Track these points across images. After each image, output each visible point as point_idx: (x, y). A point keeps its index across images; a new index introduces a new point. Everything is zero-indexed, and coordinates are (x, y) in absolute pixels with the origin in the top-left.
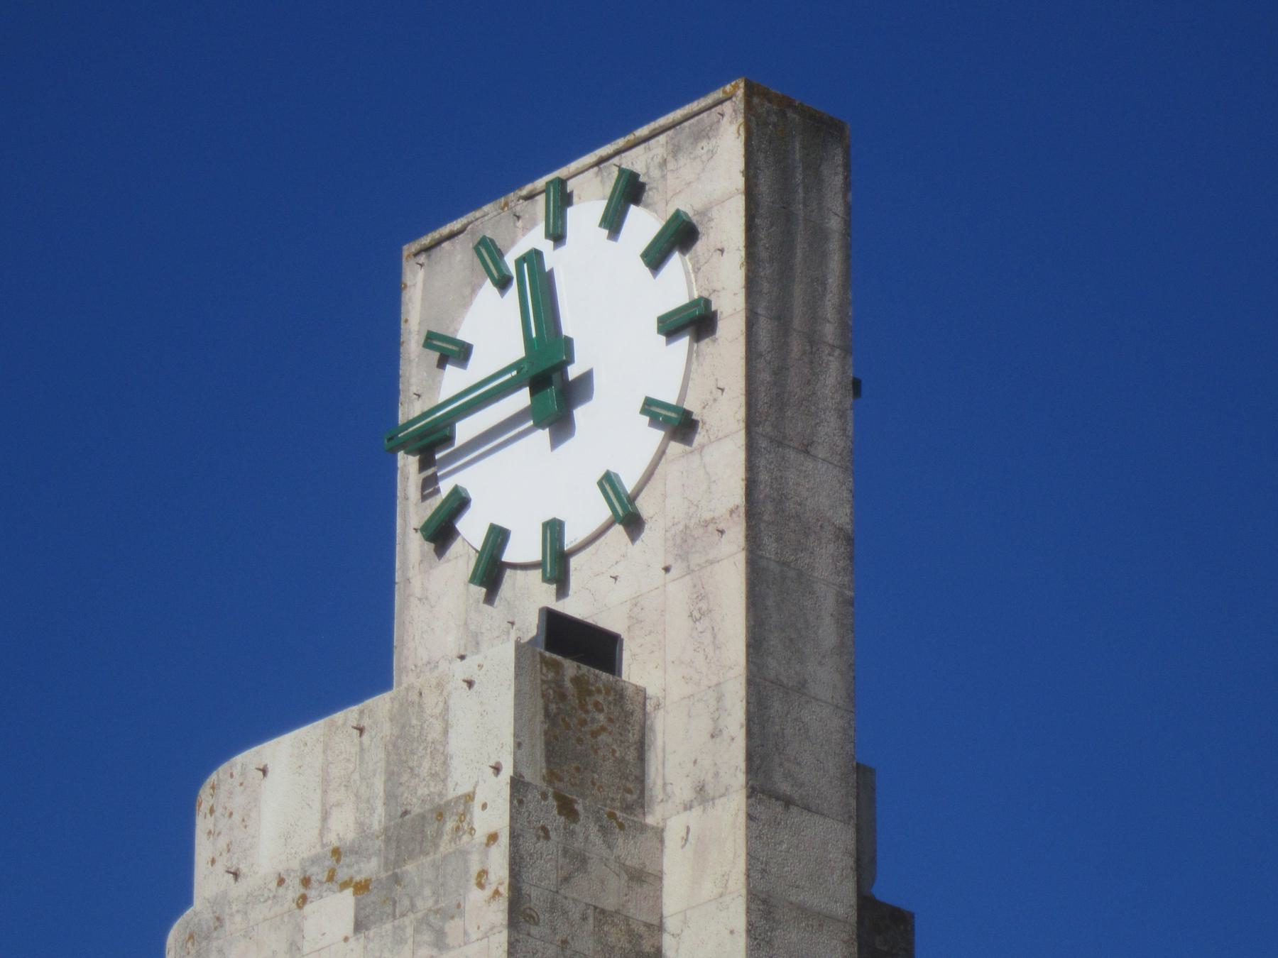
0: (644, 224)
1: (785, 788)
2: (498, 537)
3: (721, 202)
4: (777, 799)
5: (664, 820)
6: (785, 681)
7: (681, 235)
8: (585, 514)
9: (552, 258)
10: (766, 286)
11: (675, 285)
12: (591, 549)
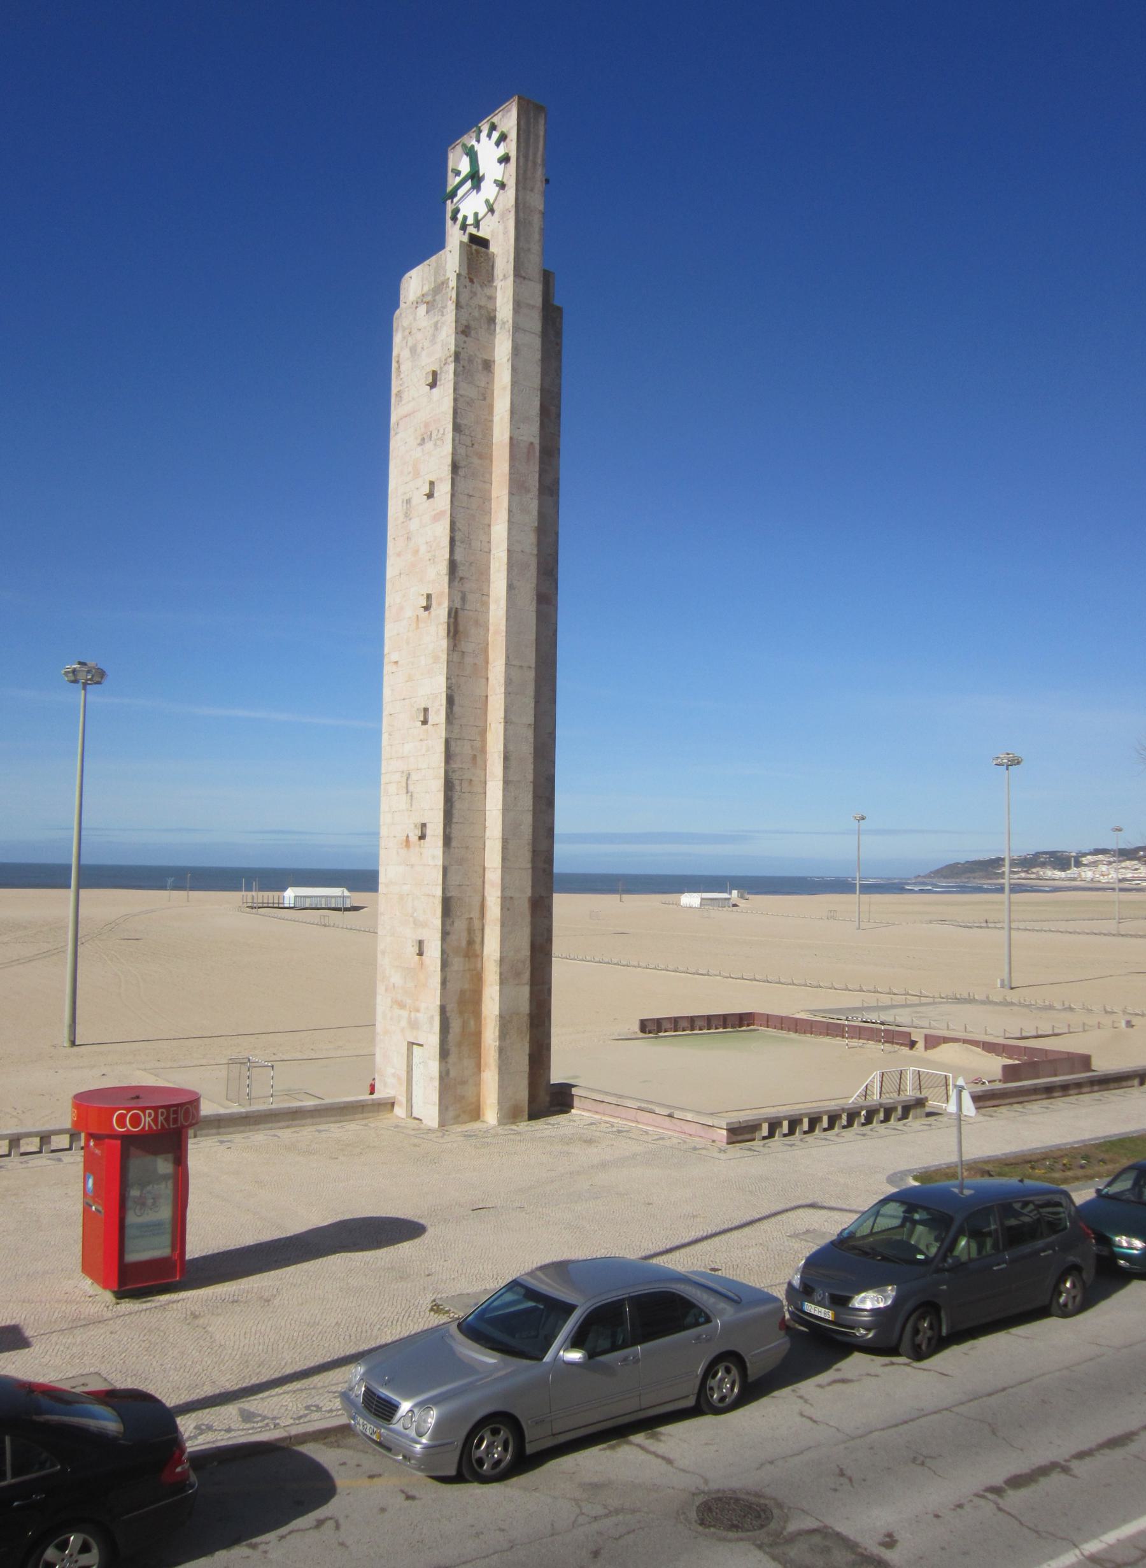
0: (496, 135)
2: (465, 218)
7: (503, 138)
8: (482, 210)
9: (477, 147)
11: (501, 151)
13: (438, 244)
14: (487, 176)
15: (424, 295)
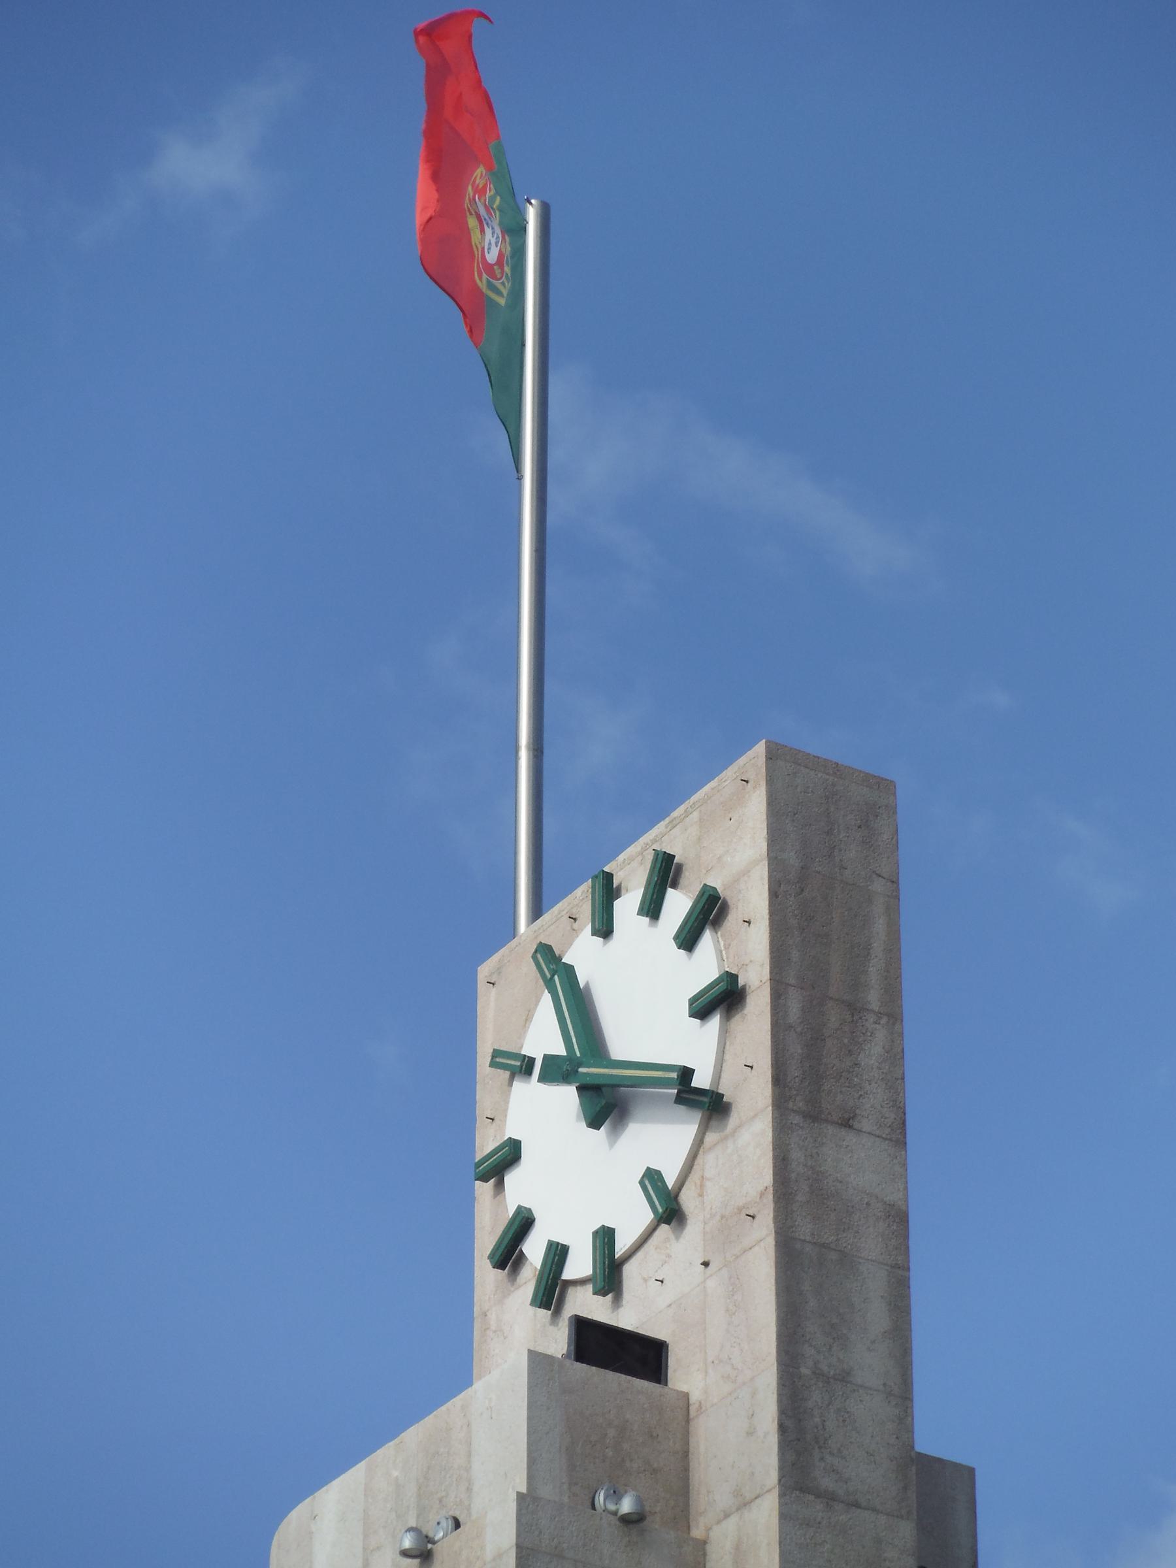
0: (678, 905)
1: (827, 1483)
2: (558, 1254)
3: (746, 872)
4: (818, 1496)
5: (708, 1529)
6: (825, 1369)
7: (710, 911)
8: (632, 1217)
10: (795, 955)
11: (705, 966)
12: (640, 1255)
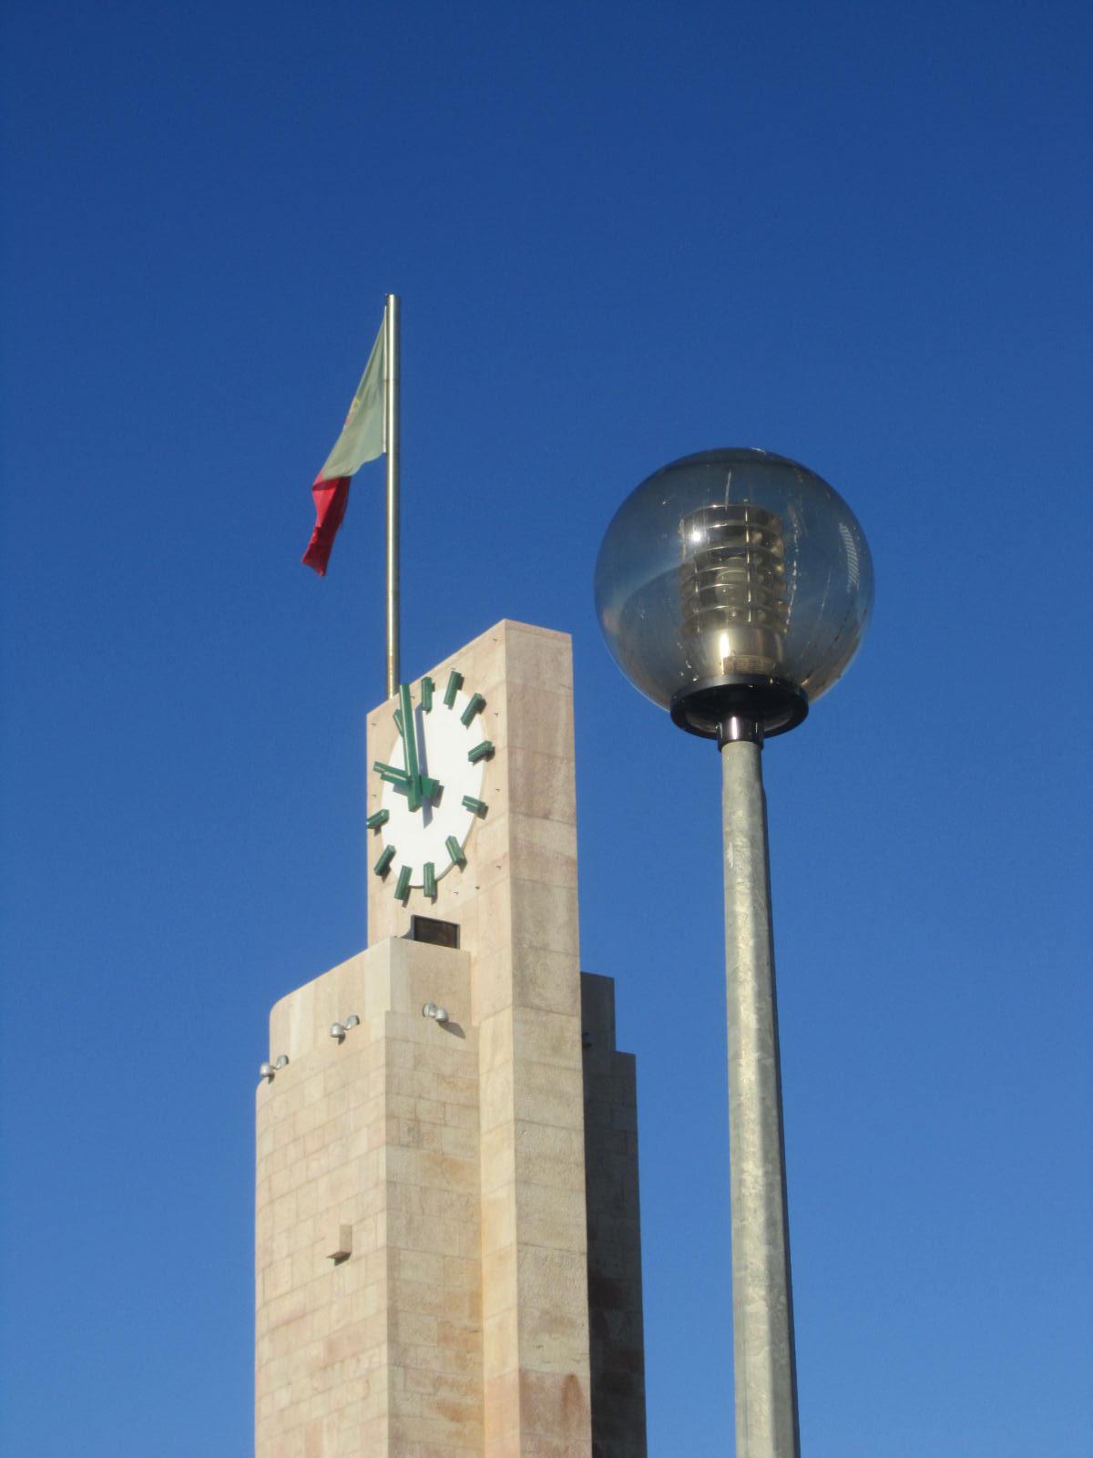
0: (463, 700)
2: (406, 872)
7: (478, 705)
8: (443, 861)
11: (477, 734)
13: (352, 938)
14: (464, 769)
15: (324, 1040)
